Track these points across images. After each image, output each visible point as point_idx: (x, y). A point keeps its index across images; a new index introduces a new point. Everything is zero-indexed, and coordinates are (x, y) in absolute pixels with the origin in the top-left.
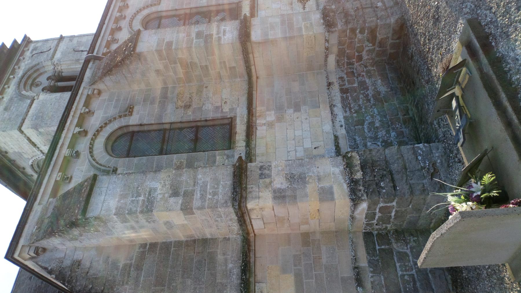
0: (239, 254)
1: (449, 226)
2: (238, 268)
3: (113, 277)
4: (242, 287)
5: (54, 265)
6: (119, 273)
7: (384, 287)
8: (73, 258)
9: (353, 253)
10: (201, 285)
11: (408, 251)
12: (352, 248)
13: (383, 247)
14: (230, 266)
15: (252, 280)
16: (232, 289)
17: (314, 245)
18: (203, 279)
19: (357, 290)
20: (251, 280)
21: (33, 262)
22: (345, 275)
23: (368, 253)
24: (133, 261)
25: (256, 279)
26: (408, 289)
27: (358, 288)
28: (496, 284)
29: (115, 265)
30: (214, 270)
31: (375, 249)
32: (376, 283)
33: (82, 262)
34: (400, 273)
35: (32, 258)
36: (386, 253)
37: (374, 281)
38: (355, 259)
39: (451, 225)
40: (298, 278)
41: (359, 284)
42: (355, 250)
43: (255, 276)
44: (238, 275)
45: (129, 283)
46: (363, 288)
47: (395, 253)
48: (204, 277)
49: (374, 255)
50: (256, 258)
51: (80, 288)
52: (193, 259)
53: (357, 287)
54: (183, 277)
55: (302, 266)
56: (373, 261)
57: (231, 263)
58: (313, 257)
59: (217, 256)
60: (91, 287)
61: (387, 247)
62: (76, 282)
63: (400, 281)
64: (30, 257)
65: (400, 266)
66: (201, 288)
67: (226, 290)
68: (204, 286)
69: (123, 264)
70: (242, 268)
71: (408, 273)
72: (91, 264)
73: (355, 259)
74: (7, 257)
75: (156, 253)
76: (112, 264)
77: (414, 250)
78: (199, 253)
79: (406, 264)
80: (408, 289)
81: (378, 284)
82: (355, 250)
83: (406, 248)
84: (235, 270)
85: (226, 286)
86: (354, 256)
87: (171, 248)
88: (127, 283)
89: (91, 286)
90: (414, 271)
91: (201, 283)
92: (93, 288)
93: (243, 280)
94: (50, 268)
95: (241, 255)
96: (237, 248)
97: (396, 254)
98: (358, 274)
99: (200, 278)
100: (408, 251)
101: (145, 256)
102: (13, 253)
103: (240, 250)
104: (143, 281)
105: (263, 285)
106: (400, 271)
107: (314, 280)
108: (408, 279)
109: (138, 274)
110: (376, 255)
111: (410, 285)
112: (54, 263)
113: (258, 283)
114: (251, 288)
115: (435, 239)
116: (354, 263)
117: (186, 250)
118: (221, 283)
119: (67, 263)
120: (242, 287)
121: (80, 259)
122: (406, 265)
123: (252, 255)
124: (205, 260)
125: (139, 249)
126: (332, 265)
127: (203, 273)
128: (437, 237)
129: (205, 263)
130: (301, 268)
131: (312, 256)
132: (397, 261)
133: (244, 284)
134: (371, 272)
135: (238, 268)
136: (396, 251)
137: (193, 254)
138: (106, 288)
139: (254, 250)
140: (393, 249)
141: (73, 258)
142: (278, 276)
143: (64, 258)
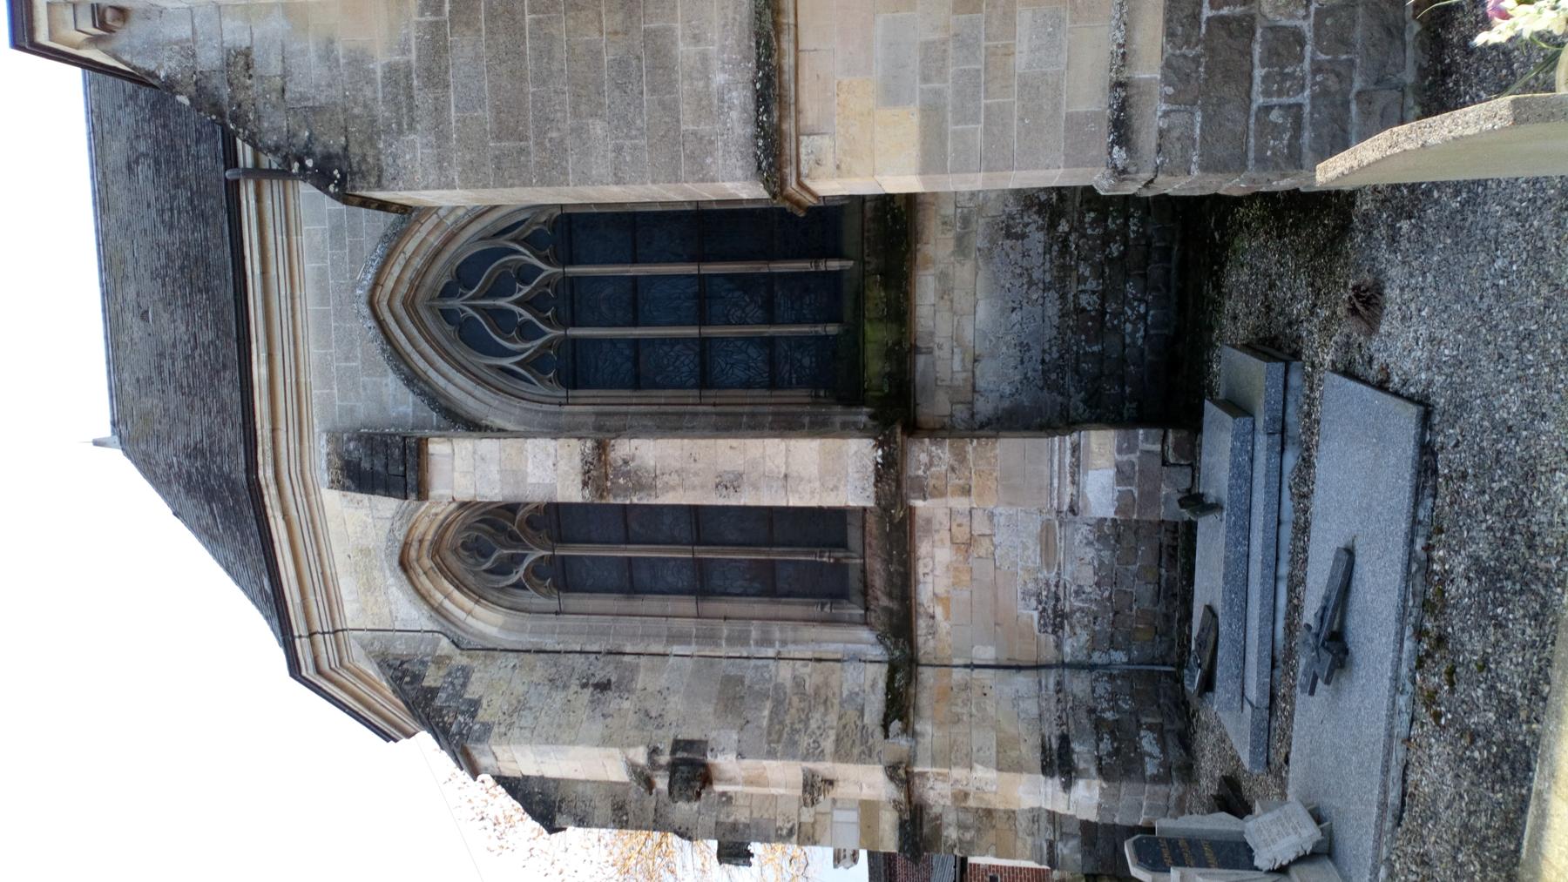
0: (746, 41)
1: (1458, 131)
2: (744, 88)
3: (365, 106)
4: (759, 147)
5: (173, 64)
6: (380, 95)
7: (1198, 145)
8: (222, 42)
9: (1118, 35)
10: (636, 137)
11: (1307, 27)
12: (1121, 15)
13: (1225, 11)
14: (719, 79)
15: (789, 126)
16: (729, 152)
17: (995, 7)
18: (638, 122)
19: (1110, 153)
20: (785, 126)
21: (104, 52)
22: (1082, 108)
23: (1170, 34)
24: (413, 56)
25: (802, 123)
26: (1269, 153)
27: (1116, 148)
28: (1550, 201)
29: (358, 61)
30: (669, 93)
31: (1196, 17)
32: (1175, 133)
33: (255, 54)
34: (1259, 100)
35: (94, 41)
36: (1230, 35)
37: (1169, 130)
38: (1124, 56)
39: (1468, 132)
40: (932, 113)
41: (1119, 136)
42: (1127, 25)
43: (798, 112)
44: (745, 110)
45: (418, 127)
46: (1129, 151)
47: (1259, 32)
48: (641, 113)
49: (1187, 42)
50: (801, 54)
51: (275, 138)
52: (599, 52)
53: (1112, 147)
54: (576, 114)
55: (945, 81)
56: (1181, 60)
57: (723, 70)
58: (986, 48)
59: (674, 43)
60: (309, 137)
61: (1239, 10)
62: (259, 118)
63: (1252, 126)
64: (84, 36)
65: (1265, 79)
66: (635, 148)
67: (712, 156)
68: (644, 142)
69: (383, 66)
70: (758, 86)
71: (1285, 100)
72: (283, 61)
73: (1124, 56)
74: (16, 44)
75: (479, 30)
76: (349, 63)
77: (1328, 22)
78: (616, 33)
79: (1286, 70)
80: (1269, 153)
81: (1178, 139)
82: (1127, 25)
83: (1302, 12)
84: (734, 94)
85: (711, 142)
86: (1120, 46)
87: (523, 15)
88: (411, 127)
89: (307, 134)
90: (1307, 92)
91: (634, 132)
92: (316, 139)
93: (762, 128)
94: (162, 74)
95: (753, 44)
96: (738, 17)
97: (1263, 35)
98: (1123, 106)
99: (630, 115)
100: (1307, 27)
101: (446, 39)
102: (31, 31)
103: (749, 24)
104: (457, 121)
105: (825, 142)
106: (1262, 93)
107: (981, 126)
108: (1280, 121)
109: (436, 99)
110: (1194, 39)
111: (1282, 139)
112: (170, 58)
113: (809, 135)
114: (788, 151)
115: (1397, 150)
116: (1118, 69)
117: (571, 22)
118: (694, 133)
119: (209, 58)
120: (759, 147)
121: (244, 46)
122: (1288, 74)
123: (787, 44)
124: (639, 58)
125: (422, 14)
126: (1045, 74)
127: (637, 101)
128: (1408, 147)
129: (640, 69)
130: (943, 85)
131: (984, 44)
132: (1260, 61)
133: (764, 138)
134: (1168, 99)
135: (744, 88)
136: (1266, 24)
137: (596, 36)
138: (352, 139)
139: (792, 27)
140: (1259, 18)
141: (222, 42)
142: (869, 114)
143: (195, 42)
